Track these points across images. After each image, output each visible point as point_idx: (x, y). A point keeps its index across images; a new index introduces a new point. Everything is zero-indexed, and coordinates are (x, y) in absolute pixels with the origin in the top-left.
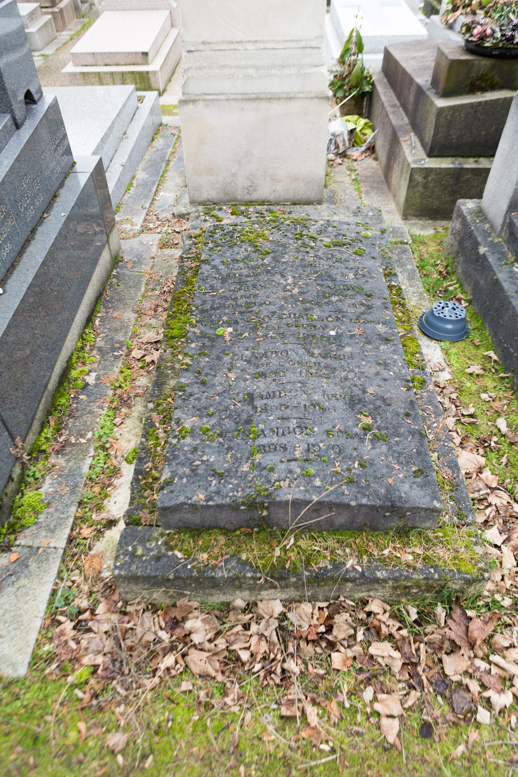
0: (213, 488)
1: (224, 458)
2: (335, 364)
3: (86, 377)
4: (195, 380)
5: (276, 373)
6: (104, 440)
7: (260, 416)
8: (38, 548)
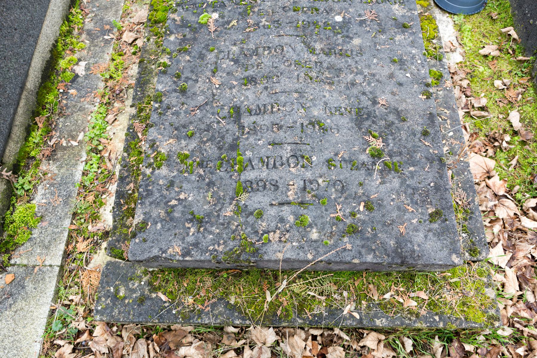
0: (190, 239)
1: (205, 197)
2: (340, 62)
3: (75, 67)
4: (174, 87)
5: (268, 78)
6: (95, 143)
7: (247, 139)
8: (34, 267)
